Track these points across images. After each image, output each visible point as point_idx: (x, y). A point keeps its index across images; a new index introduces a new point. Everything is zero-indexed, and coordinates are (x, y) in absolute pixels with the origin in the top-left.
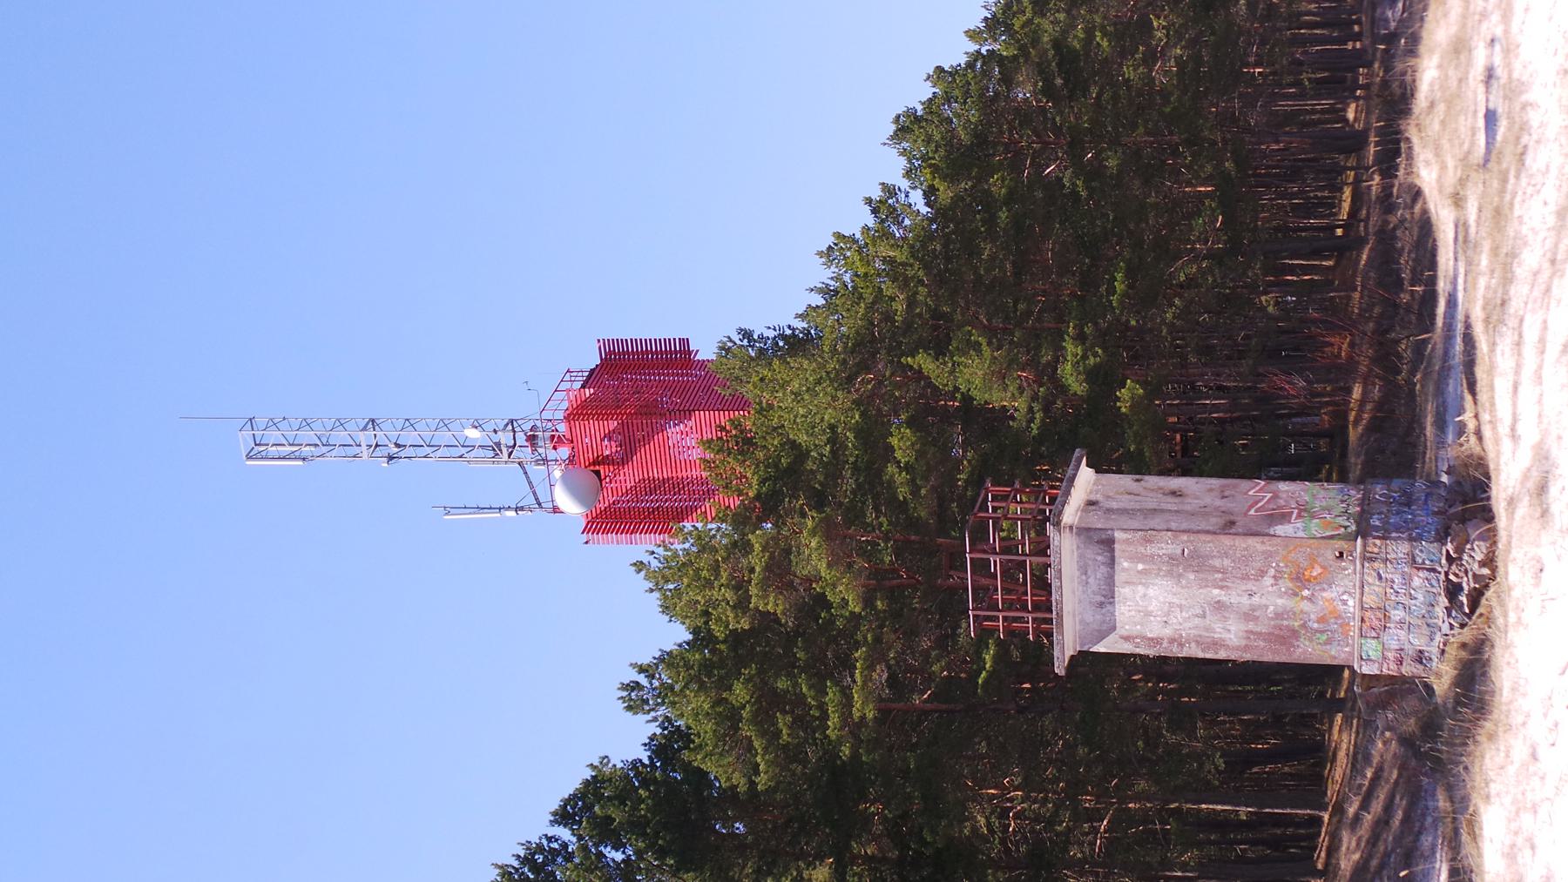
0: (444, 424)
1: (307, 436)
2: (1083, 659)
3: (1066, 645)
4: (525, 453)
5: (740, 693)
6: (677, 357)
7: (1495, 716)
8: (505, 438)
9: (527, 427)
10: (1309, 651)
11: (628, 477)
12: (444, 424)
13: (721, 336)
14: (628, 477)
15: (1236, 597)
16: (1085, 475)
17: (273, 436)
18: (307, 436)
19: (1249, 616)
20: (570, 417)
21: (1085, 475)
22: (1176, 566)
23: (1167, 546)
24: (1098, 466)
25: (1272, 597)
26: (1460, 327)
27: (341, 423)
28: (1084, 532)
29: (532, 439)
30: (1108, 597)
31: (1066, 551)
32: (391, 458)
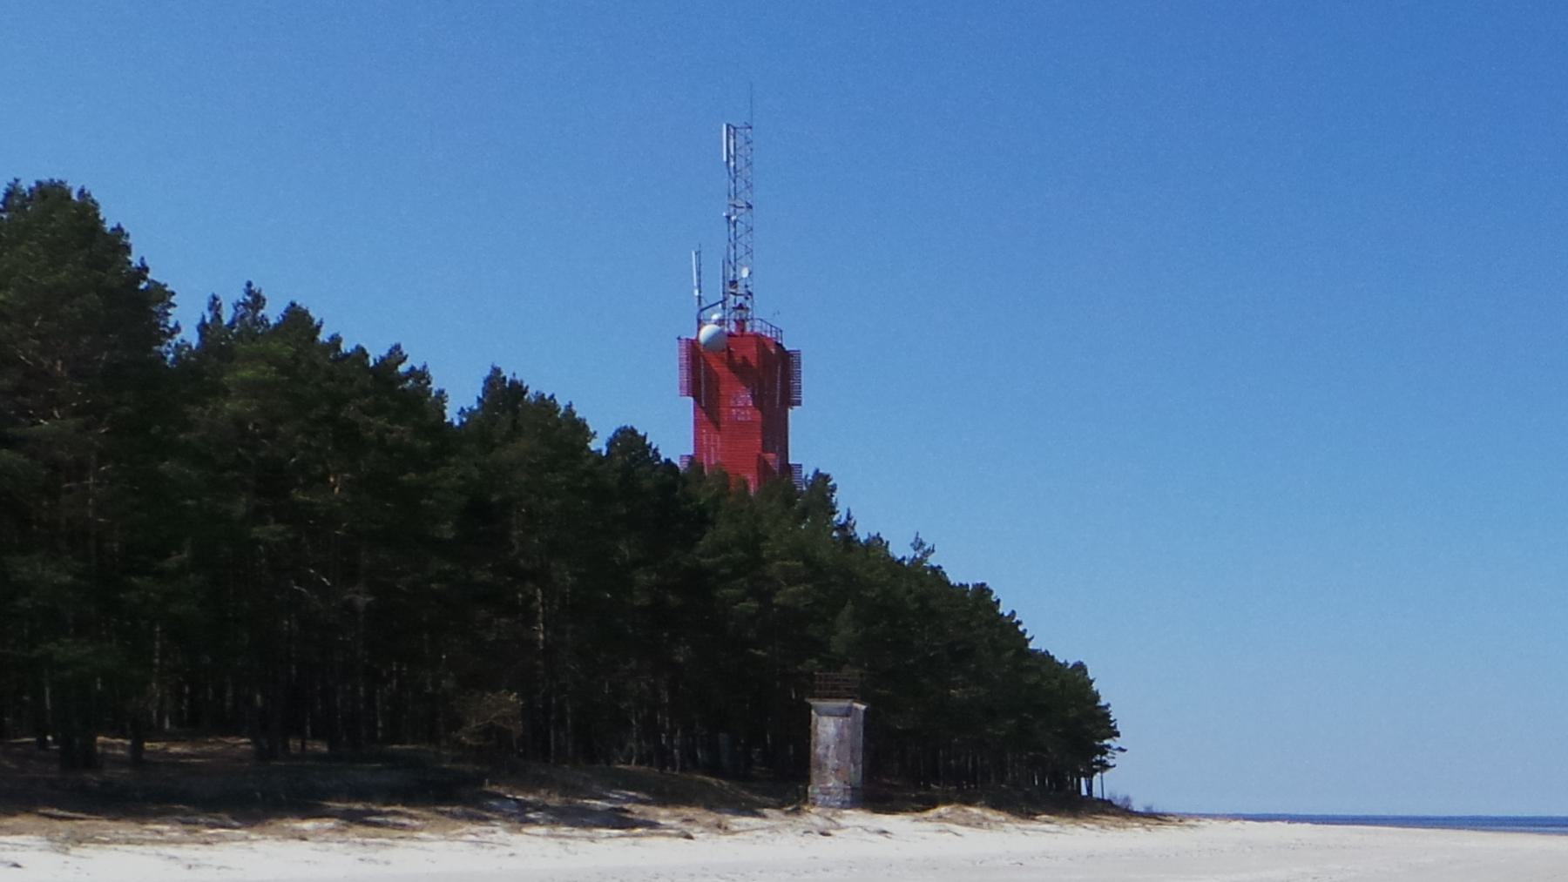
0: (749, 252)
1: (741, 163)
2: (810, 707)
3: (814, 703)
4: (731, 303)
5: (740, 554)
6: (789, 397)
7: (516, 838)
8: (741, 290)
9: (748, 305)
10: (815, 772)
11: (721, 369)
12: (749, 252)
13: (833, 475)
14: (721, 369)
15: (831, 753)
16: (863, 707)
17: (741, 141)
18: (741, 163)
19: (826, 756)
20: (758, 336)
21: (863, 707)
22: (840, 735)
23: (846, 732)
24: (866, 712)
25: (832, 762)
26: (406, 821)
27: (749, 186)
28: (850, 708)
29: (741, 307)
30: (829, 714)
31: (845, 704)
32: (728, 217)
